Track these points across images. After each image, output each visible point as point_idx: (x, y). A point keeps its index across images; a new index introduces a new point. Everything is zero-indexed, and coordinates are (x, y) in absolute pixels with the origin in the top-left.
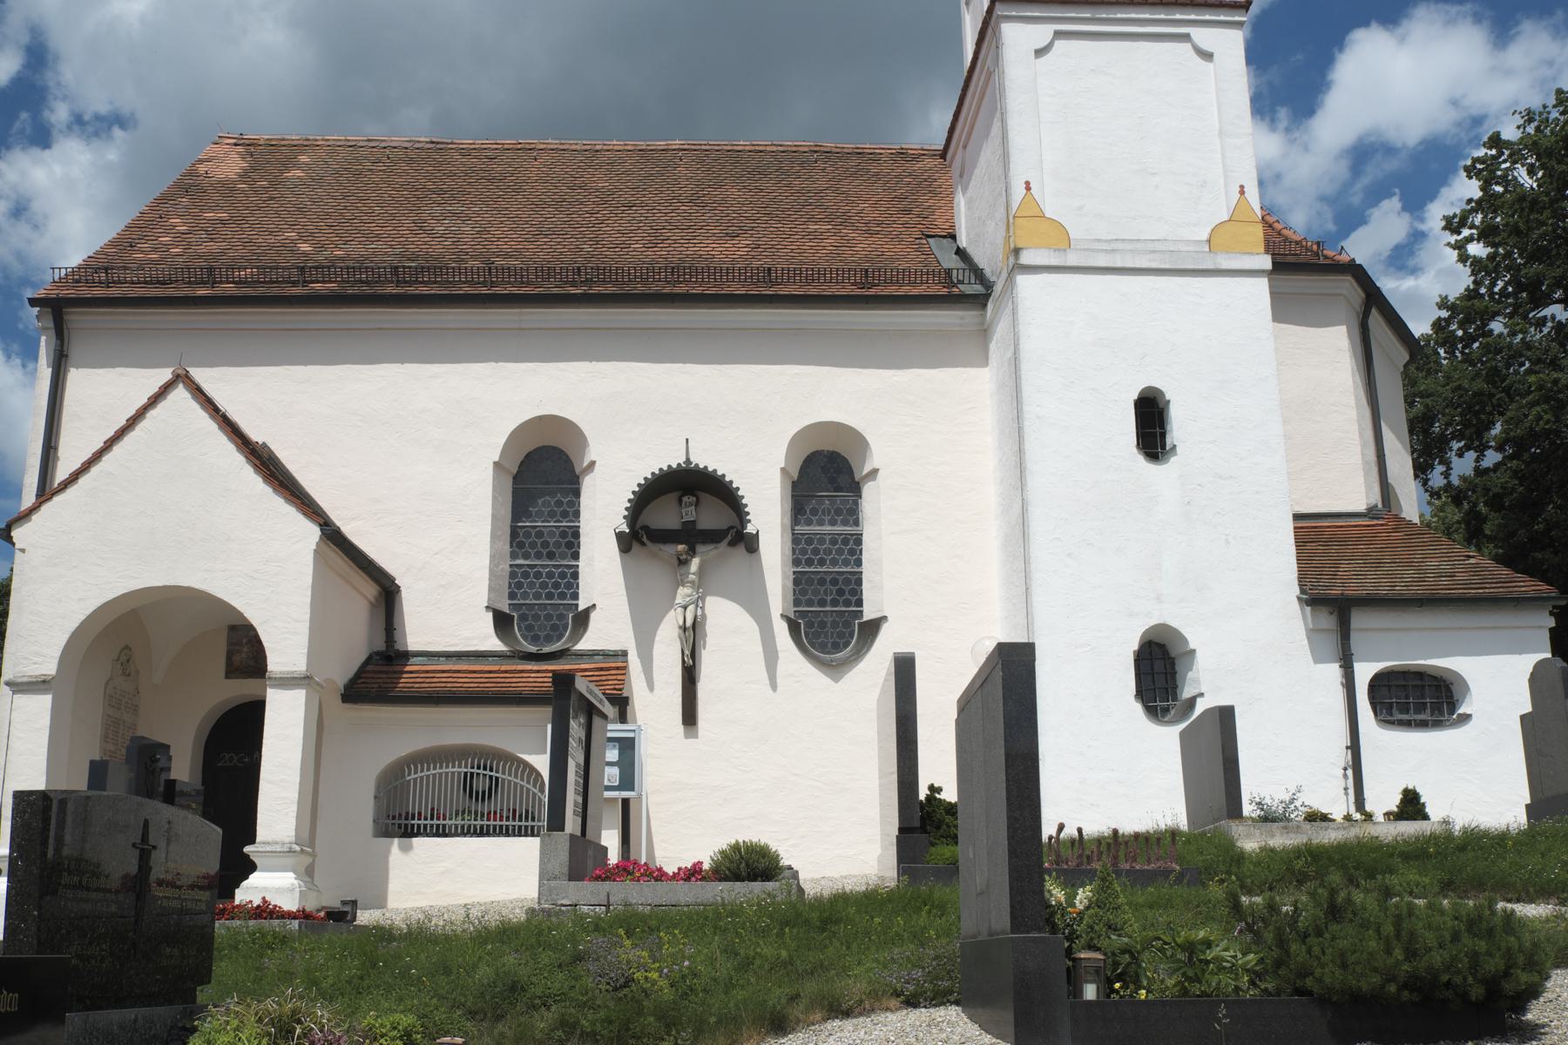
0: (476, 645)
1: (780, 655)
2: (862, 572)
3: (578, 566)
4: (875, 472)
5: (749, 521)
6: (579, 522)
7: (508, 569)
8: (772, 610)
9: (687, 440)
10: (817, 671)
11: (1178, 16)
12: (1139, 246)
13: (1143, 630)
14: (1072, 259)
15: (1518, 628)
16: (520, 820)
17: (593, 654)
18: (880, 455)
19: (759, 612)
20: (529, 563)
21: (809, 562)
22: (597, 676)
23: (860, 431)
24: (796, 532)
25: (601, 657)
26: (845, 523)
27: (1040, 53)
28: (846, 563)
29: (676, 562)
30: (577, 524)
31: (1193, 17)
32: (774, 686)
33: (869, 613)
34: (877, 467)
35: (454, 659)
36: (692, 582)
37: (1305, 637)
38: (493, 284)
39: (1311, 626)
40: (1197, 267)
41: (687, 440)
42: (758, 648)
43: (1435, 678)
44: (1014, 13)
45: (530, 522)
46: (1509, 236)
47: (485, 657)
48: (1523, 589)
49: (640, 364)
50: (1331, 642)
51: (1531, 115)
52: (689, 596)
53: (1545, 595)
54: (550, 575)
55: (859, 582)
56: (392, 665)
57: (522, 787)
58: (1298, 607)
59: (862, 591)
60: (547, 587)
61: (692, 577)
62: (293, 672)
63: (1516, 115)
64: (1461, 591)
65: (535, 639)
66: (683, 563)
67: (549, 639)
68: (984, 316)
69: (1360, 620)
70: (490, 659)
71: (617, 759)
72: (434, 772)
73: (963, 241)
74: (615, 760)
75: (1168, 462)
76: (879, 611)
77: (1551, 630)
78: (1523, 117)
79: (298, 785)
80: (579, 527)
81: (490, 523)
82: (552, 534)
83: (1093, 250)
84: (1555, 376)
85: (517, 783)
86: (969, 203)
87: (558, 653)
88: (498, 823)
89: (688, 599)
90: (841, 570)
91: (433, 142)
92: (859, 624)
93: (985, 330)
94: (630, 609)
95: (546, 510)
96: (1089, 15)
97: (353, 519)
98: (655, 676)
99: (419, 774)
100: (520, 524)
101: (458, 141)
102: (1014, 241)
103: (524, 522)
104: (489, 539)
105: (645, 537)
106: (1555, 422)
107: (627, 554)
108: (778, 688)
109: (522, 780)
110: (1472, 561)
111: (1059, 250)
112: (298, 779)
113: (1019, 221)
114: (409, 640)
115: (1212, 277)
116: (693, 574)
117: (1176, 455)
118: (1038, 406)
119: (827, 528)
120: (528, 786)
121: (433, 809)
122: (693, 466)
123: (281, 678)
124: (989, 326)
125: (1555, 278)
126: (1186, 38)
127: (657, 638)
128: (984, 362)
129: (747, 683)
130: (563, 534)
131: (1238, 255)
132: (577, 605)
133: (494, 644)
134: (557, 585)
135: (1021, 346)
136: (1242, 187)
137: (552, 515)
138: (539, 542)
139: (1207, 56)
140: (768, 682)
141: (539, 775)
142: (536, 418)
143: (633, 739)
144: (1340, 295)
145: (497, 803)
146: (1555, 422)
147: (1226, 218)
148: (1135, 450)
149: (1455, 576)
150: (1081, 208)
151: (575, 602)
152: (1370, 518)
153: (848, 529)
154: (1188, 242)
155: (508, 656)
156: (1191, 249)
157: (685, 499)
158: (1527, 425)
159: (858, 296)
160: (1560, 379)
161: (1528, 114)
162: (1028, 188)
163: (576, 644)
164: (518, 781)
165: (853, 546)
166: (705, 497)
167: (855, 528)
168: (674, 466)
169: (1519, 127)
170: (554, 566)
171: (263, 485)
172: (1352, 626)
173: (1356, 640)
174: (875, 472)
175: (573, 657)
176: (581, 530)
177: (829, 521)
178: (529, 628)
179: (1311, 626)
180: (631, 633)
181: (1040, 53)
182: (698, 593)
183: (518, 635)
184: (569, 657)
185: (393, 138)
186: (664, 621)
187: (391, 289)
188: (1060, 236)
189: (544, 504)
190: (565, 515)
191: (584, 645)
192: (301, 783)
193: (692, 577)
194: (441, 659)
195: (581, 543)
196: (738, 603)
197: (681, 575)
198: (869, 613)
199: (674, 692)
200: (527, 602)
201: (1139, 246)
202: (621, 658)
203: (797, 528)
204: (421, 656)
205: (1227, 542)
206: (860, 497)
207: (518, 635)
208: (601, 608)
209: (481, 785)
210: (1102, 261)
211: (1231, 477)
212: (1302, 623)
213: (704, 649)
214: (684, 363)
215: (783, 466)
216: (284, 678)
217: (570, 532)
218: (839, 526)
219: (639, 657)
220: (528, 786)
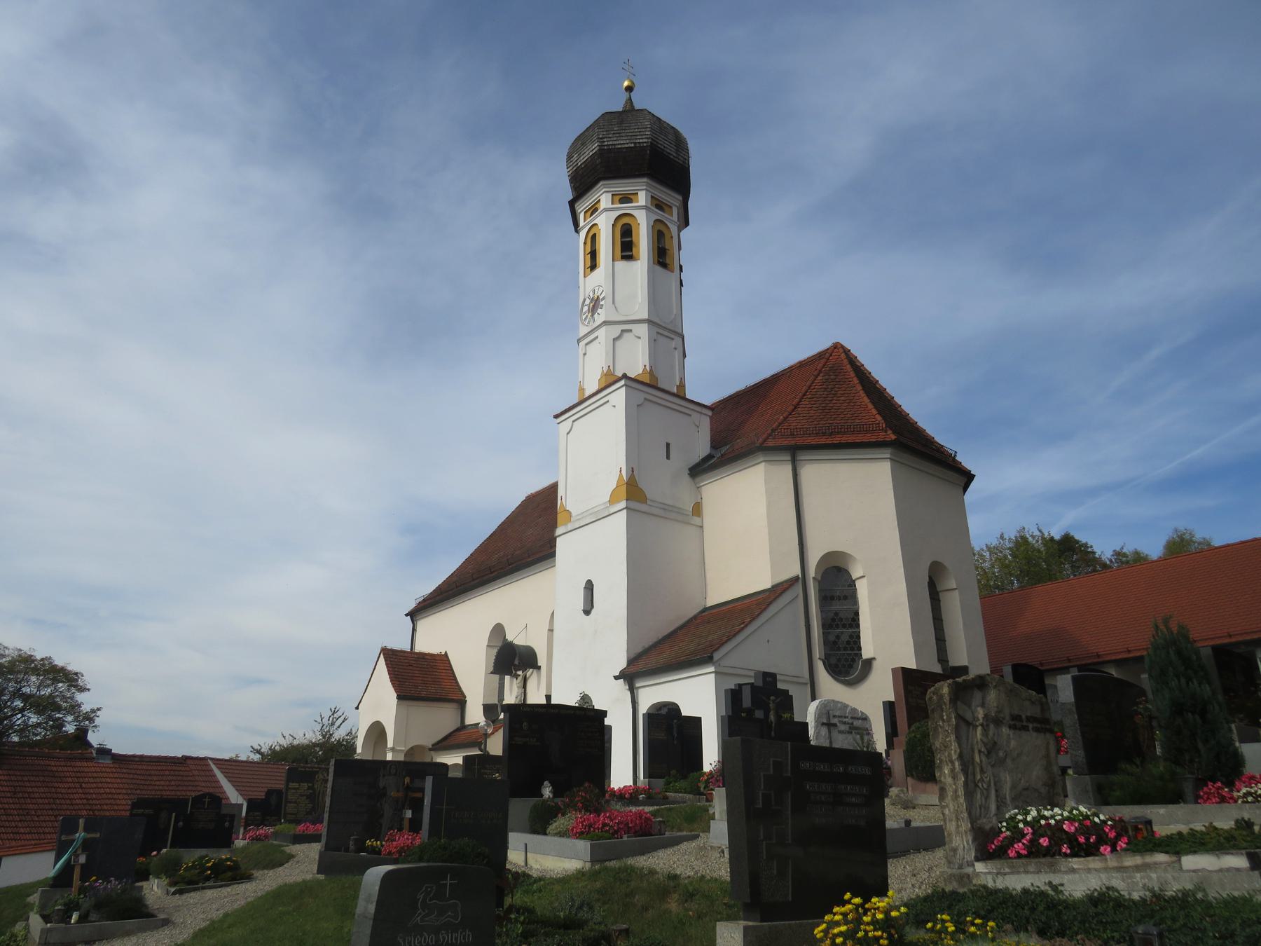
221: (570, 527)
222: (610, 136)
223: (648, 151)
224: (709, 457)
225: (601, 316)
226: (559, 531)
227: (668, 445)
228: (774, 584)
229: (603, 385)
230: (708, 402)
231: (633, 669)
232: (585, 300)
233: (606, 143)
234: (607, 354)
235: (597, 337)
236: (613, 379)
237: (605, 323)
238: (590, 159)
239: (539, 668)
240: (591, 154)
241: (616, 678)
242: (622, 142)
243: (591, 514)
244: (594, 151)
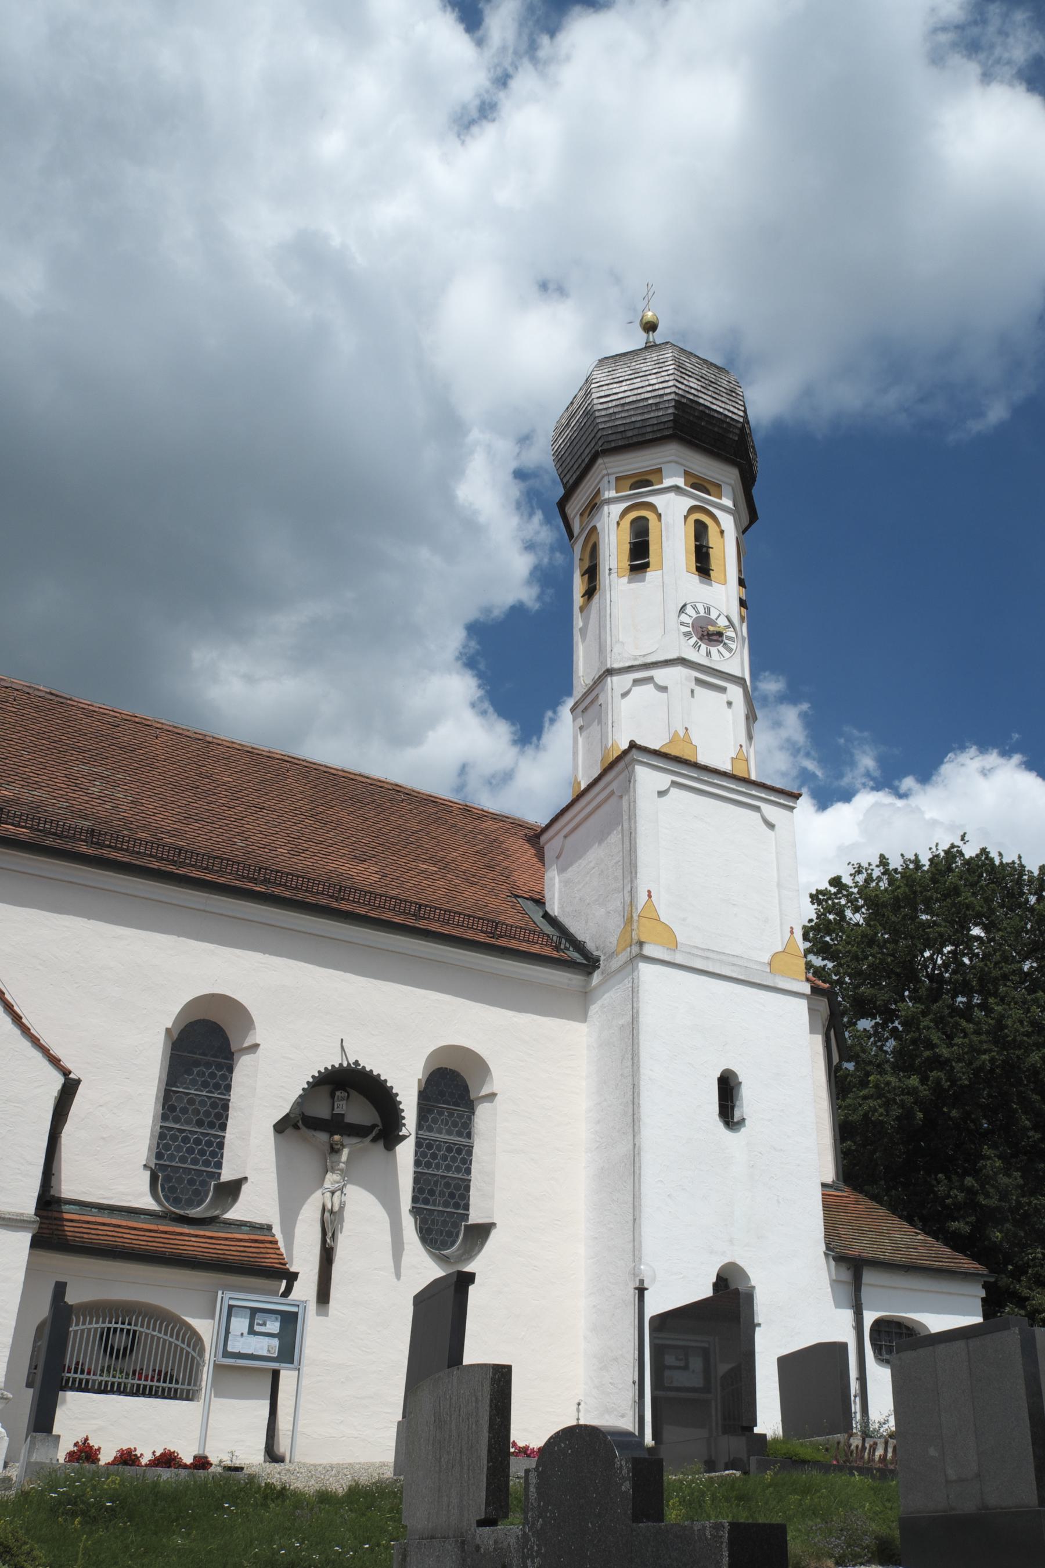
0: (130, 1201)
1: (406, 1247)
2: (470, 1180)
3: (224, 1137)
4: (492, 1096)
5: (404, 1125)
6: (230, 1096)
8: (402, 1204)
9: (342, 1040)
10: (435, 1265)
12: (724, 957)
13: (720, 1266)
14: (679, 959)
15: (963, 1295)
16: (152, 1380)
17: (240, 1224)
18: (499, 1080)
19: (389, 1201)
20: (179, 1127)
21: (428, 1165)
22: (254, 1247)
23: (484, 1058)
24: (419, 1136)
25: (248, 1228)
26: (460, 1134)
27: (661, 794)
28: (458, 1170)
29: (327, 1148)
30: (227, 1097)
32: (398, 1275)
33: (475, 1217)
34: (496, 1092)
35: (106, 1212)
36: (342, 1170)
37: (829, 1285)
38: (182, 864)
39: (834, 1278)
40: (762, 983)
41: (342, 1040)
42: (388, 1238)
43: (908, 1328)
44: (645, 760)
45: (184, 1088)
46: (851, 961)
47: (137, 1213)
48: (966, 1266)
49: (306, 965)
50: (847, 1291)
51: (861, 869)
52: (338, 1183)
53: (980, 1272)
54: (198, 1142)
55: (467, 1188)
56: (48, 1210)
57: (182, 1349)
58: (825, 1261)
59: (469, 1196)
60: (193, 1153)
61: (342, 1165)
62: (22, 1214)
63: (850, 866)
64: (947, 1264)
65: (176, 1202)
66: (335, 1150)
67: (190, 1204)
68: (589, 982)
70: (142, 1216)
71: (278, 1331)
72: (95, 1326)
73: (555, 908)
74: (276, 1332)
75: (739, 1131)
76: (490, 1217)
77: (983, 1299)
78: (854, 868)
79: (13, 1330)
80: (229, 1100)
81: (156, 1085)
82: (203, 1103)
83: (693, 954)
84: (888, 1079)
85: (172, 1342)
86: (566, 883)
87: (208, 1220)
88: (167, 1385)
89: (337, 1185)
90: (454, 1176)
91: (52, 694)
92: (465, 1226)
93: (586, 993)
94: (278, 1186)
95: (200, 1080)
99: (81, 1327)
100: (174, 1089)
101: (76, 699)
102: (638, 935)
103: (178, 1087)
104: (154, 1100)
105: (300, 1122)
106: (886, 1116)
107: (281, 1135)
108: (402, 1278)
109: (189, 1345)
110: (920, 1237)
112: (13, 1324)
113: (642, 920)
114: (62, 1187)
115: (795, 997)
116: (344, 1163)
117: (745, 1126)
118: (651, 1070)
119: (443, 1137)
120: (188, 1349)
121: (77, 1363)
122: (360, 1067)
123: (10, 1219)
124: (591, 991)
125: (884, 1000)
126: (757, 809)
127: (300, 1217)
128: (583, 1017)
129: (376, 1269)
130: (214, 1105)
131: (789, 979)
132: (220, 1174)
134: (202, 1153)
135: (641, 1020)
137: (205, 1085)
138: (191, 1108)
140: (393, 1270)
141: (200, 1339)
142: (210, 994)
143: (296, 1314)
144: (818, 1011)
145: (134, 1361)
146: (886, 1116)
147: (780, 949)
148: (717, 1118)
149: (917, 1249)
150: (684, 920)
151: (219, 1171)
152: (835, 1189)
153: (462, 1140)
155: (160, 1216)
156: (758, 968)
157: (338, 1093)
158: (862, 1113)
160: (891, 1082)
161: (859, 868)
162: (650, 896)
163: (226, 1212)
164: (179, 1343)
166: (354, 1094)
167: (468, 1140)
169: (851, 875)
170: (202, 1134)
171: (12, 1026)
172: (863, 1281)
173: (865, 1293)
174: (492, 1096)
175: (222, 1225)
176: (230, 1104)
177: (447, 1130)
178: (173, 1189)
179: (834, 1278)
180: (277, 1209)
181: (661, 794)
182: (344, 1181)
183: (161, 1195)
184: (218, 1225)
185: (12, 680)
186: (307, 1203)
187: (83, 848)
188: (671, 941)
189: (198, 1074)
190: (217, 1087)
191: (235, 1213)
192: (16, 1328)
193: (342, 1165)
194: (93, 1210)
195: (230, 1116)
196: (373, 1193)
197: (332, 1162)
198: (475, 1217)
199: (311, 1270)
200: (173, 1164)
201: (724, 957)
202: (266, 1232)
204: (74, 1205)
205: (778, 1202)
206: (474, 1113)
207: (161, 1195)
208: (252, 1182)
209: (119, 1341)
211: (781, 1150)
212: (827, 1273)
213: (341, 1233)
214: (345, 971)
215: (420, 1077)
216: (13, 1219)
217: (221, 1103)
218: (425, 1132)
219: (282, 1233)
220: (188, 1349)
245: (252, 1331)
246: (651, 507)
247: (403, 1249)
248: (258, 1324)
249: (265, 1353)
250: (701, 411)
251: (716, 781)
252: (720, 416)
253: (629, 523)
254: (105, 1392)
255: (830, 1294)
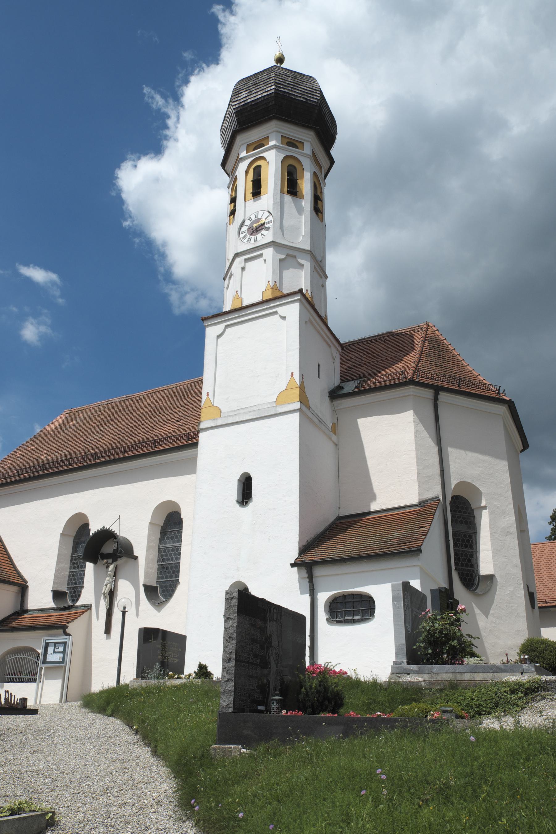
7: (68, 573)
11: (272, 305)
17: (82, 606)
31: (278, 303)
32: (137, 616)
37: (298, 582)
50: (306, 583)
69: (318, 572)
96: (237, 315)
97: (19, 561)
98: (99, 614)
111: (215, 419)
115: (275, 417)
126: (276, 313)
133: (52, 605)
136: (292, 373)
139: (284, 318)
144: (411, 395)
150: (227, 399)
154: (267, 404)
156: (268, 406)
159: (101, 462)
162: (208, 395)
165: (178, 549)
168: (99, 530)
196: (129, 581)
203: (161, 546)
205: (269, 540)
210: (231, 420)
221: (220, 422)
222: (286, 85)
223: (316, 111)
224: (340, 388)
225: (265, 237)
226: (202, 426)
227: (319, 366)
228: (420, 501)
229: (270, 297)
230: (342, 341)
231: (310, 557)
232: (244, 222)
233: (282, 89)
234: (274, 271)
235: (261, 255)
236: (278, 294)
237: (273, 244)
238: (262, 99)
239: (136, 558)
240: (264, 94)
241: (292, 565)
242: (295, 94)
243: (251, 412)
244: (269, 93)
245: (55, 652)
246: (263, 158)
247: (140, 603)
248: (57, 649)
249: (58, 660)
250: (250, 105)
251: (249, 312)
252: (260, 100)
253: (280, 162)
254: (21, 682)
255: (298, 587)
